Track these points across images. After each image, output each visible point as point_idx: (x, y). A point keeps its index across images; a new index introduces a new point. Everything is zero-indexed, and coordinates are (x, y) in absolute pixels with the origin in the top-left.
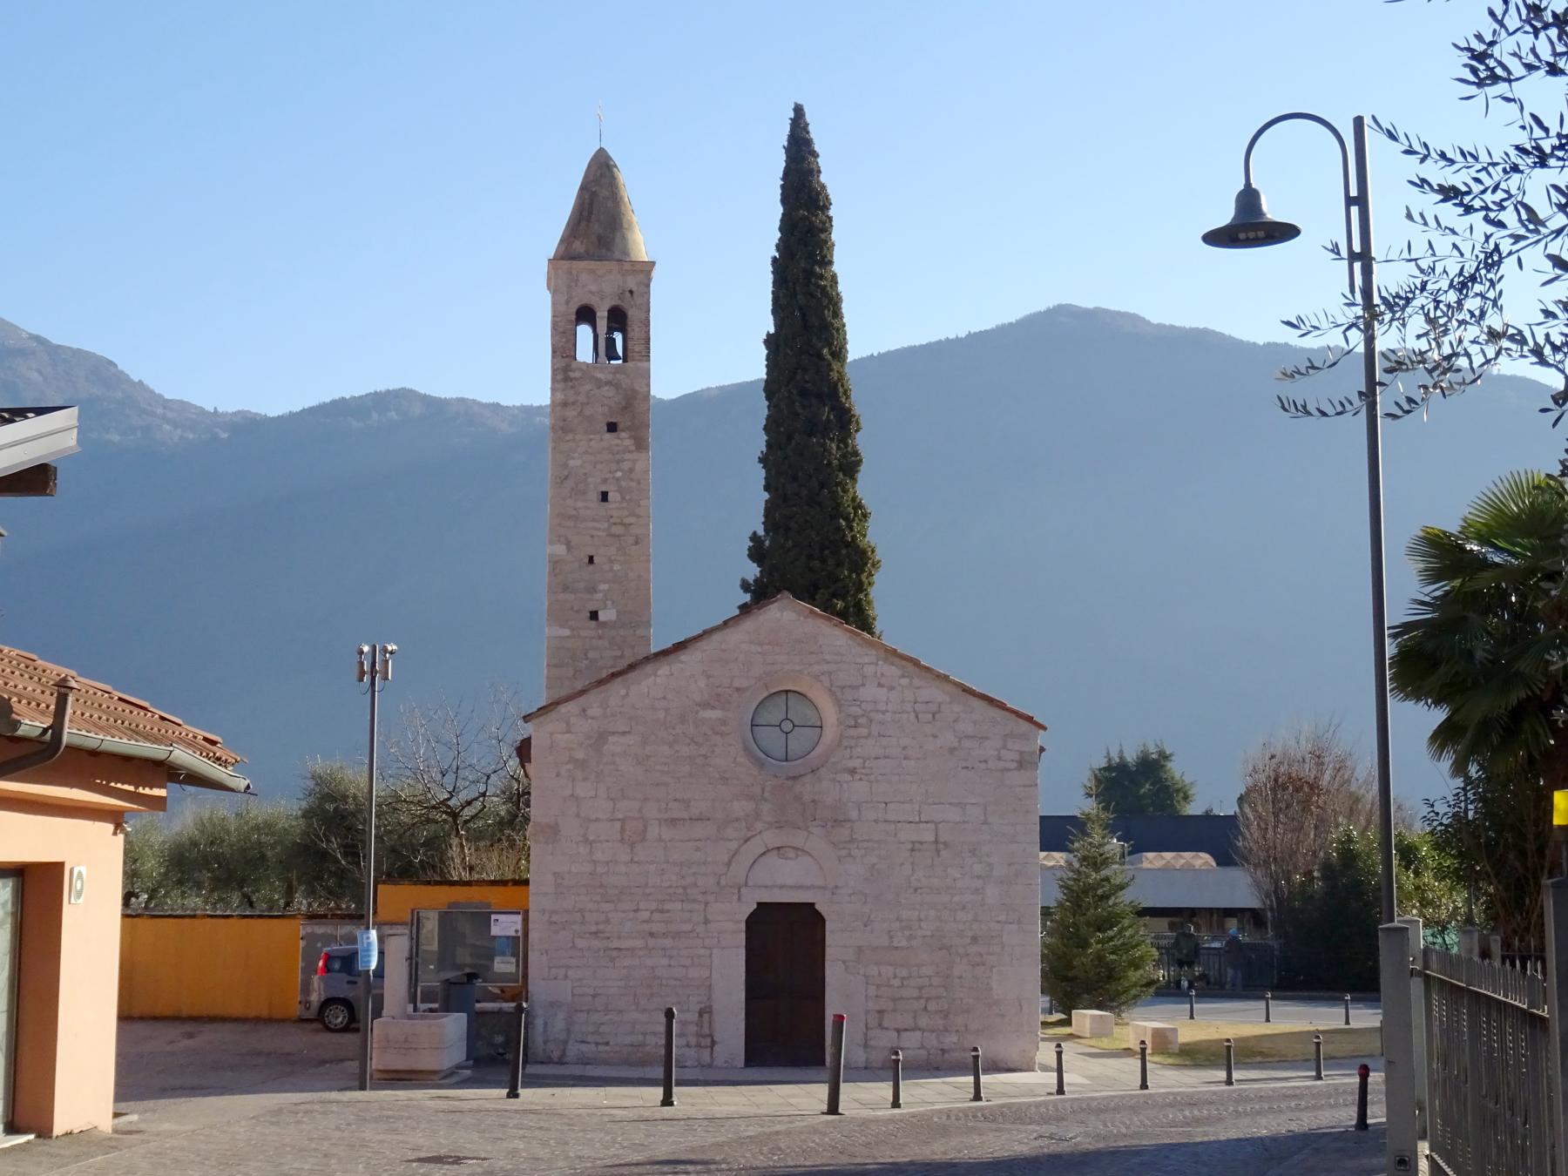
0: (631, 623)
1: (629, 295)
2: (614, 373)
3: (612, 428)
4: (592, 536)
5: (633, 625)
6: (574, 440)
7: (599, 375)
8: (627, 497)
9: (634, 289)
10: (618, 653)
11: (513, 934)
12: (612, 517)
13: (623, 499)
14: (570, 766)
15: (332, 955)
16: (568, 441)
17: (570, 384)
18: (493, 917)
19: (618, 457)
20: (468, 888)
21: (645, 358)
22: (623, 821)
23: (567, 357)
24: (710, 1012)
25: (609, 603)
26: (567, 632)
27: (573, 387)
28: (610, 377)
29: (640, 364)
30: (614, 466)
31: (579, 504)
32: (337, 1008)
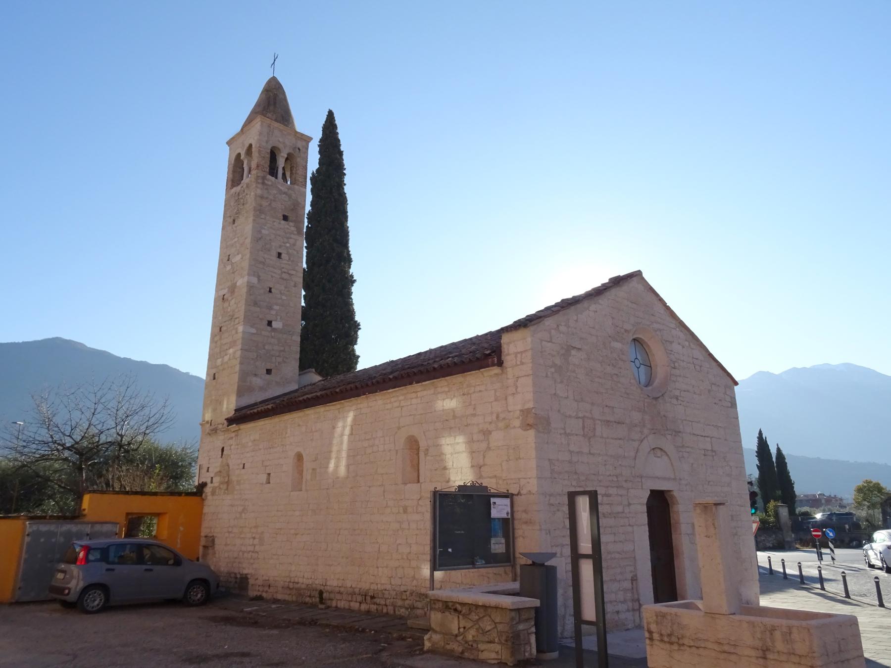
0: (290, 332)
1: (298, 150)
2: (288, 189)
3: (285, 218)
4: (272, 276)
5: (290, 333)
6: (265, 219)
7: (281, 188)
8: (292, 259)
9: (301, 148)
10: (282, 348)
11: (505, 516)
12: (283, 268)
13: (289, 259)
14: (553, 370)
15: (93, 547)
16: (262, 218)
17: (266, 187)
18: (492, 500)
19: (288, 235)
20: (155, 497)
21: (304, 186)
22: (583, 418)
23: (264, 171)
24: (636, 580)
25: (279, 317)
26: (253, 331)
27: (267, 189)
28: (286, 190)
29: (301, 188)
30: (286, 240)
31: (266, 256)
32: (95, 593)
